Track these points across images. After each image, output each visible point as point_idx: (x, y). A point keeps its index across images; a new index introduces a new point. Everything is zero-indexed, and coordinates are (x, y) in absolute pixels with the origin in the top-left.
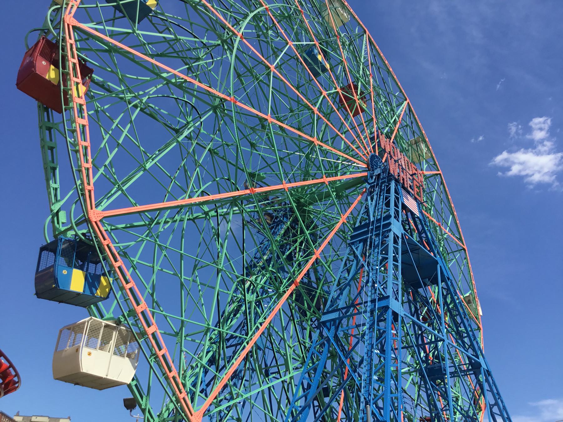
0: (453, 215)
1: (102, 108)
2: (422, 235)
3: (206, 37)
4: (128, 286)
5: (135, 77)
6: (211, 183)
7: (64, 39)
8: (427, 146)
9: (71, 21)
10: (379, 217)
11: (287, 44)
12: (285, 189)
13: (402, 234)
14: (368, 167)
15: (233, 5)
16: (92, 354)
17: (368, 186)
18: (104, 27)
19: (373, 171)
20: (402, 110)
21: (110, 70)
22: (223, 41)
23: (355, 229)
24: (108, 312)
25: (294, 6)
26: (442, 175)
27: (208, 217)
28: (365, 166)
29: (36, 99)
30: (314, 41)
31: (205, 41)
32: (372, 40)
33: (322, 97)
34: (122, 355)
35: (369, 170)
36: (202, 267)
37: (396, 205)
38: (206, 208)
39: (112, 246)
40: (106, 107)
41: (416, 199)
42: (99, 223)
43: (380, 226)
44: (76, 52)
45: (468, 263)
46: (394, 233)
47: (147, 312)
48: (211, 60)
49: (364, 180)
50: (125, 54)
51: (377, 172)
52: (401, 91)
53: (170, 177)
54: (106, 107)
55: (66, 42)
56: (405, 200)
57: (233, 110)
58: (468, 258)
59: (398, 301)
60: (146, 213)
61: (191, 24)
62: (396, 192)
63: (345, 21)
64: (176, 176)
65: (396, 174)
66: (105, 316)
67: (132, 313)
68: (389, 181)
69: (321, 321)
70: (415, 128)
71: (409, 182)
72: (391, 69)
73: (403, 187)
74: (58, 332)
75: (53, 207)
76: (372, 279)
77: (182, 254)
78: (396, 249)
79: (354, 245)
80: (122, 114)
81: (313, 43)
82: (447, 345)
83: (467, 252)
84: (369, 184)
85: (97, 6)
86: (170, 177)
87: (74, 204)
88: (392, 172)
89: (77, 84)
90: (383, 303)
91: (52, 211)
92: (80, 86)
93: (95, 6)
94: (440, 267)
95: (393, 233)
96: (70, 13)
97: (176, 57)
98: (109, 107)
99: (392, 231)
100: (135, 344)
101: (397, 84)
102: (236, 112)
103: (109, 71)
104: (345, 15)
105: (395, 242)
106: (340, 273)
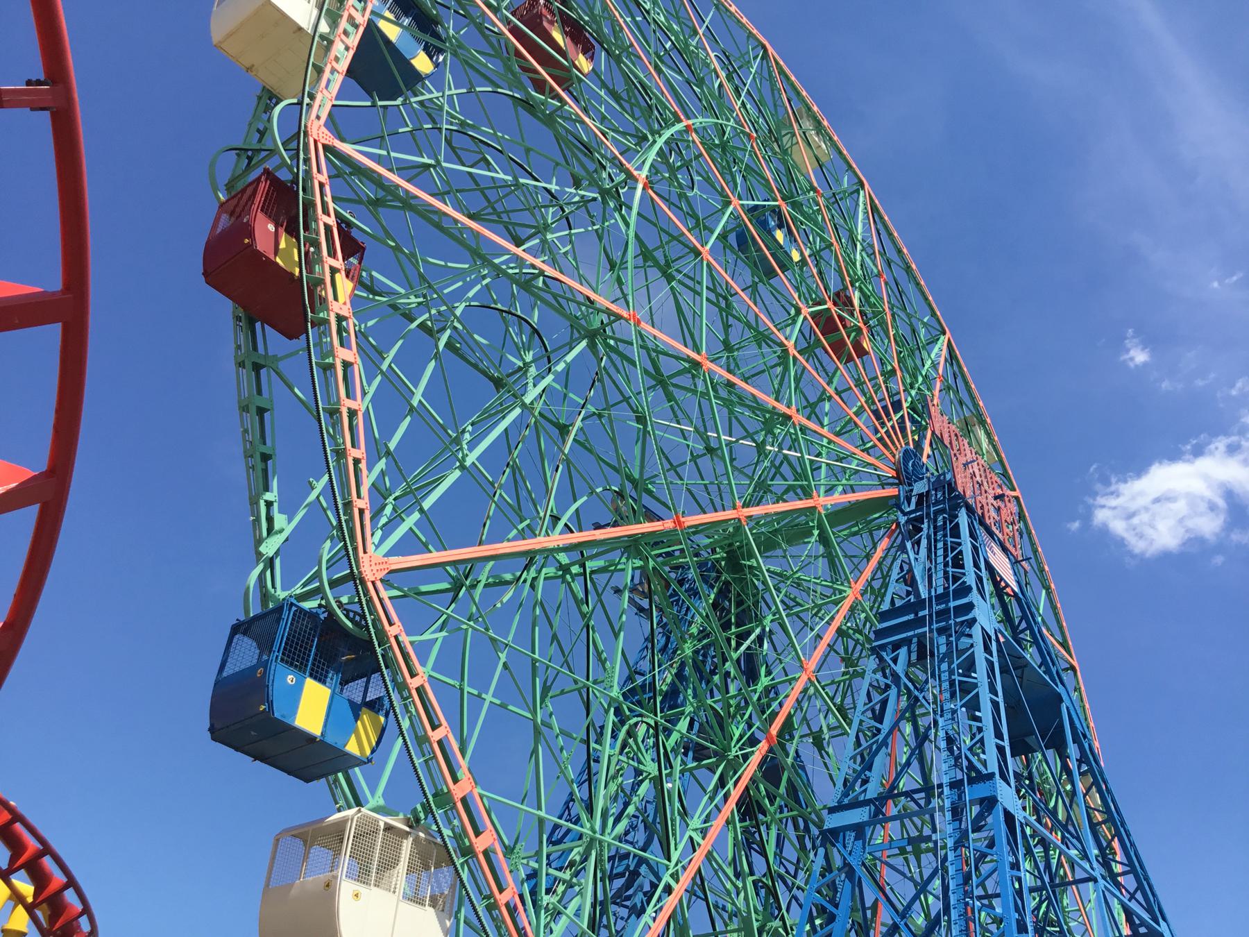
0: (1048, 589)
1: (363, 326)
2: (1021, 636)
3: (554, 180)
4: (435, 736)
5: (443, 263)
6: (585, 498)
7: (308, 173)
8: (988, 435)
9: (321, 135)
10: (940, 591)
11: (730, 203)
12: (739, 520)
13: (995, 630)
14: (898, 477)
15: (606, 118)
16: (362, 898)
17: (903, 520)
18: (388, 153)
19: (910, 485)
20: (939, 350)
21: (393, 244)
22: (604, 193)
23: (883, 616)
24: (373, 793)
25: (732, 123)
26: (1021, 500)
27: (568, 577)
28: (891, 473)
29: (64, 284)
30: (777, 200)
31: (553, 187)
32: (877, 202)
33: (801, 318)
34: (421, 902)
35: (900, 483)
36: (562, 692)
37: (976, 565)
38: (563, 558)
39: (406, 640)
40: (370, 323)
41: (1005, 550)
42: (379, 584)
43: (947, 611)
44: (331, 205)
45: (1082, 701)
46: (982, 628)
47: (473, 798)
48: (567, 232)
49: (893, 504)
50: (428, 214)
51: (920, 487)
52: (933, 314)
53: (492, 484)
54: (370, 323)
55: (312, 179)
56: (990, 554)
57: (634, 341)
58: (1083, 688)
59: (1011, 787)
60: (448, 568)
61: (528, 151)
62: (973, 535)
63: (823, 159)
64: (503, 482)
65: (969, 493)
66: (367, 802)
67: (443, 798)
68: (956, 507)
69: (825, 827)
70: (964, 395)
71: (993, 514)
72: (914, 266)
73: (982, 523)
74: (272, 841)
75: (262, 549)
76: (947, 733)
77: (537, 661)
78: (995, 705)
79: (886, 651)
80: (400, 342)
81: (777, 203)
82: (1103, 892)
83: (1079, 674)
84: (905, 514)
85: (374, 106)
86: (492, 484)
87: (329, 541)
88: (960, 489)
89: (334, 271)
90: (982, 790)
91: (260, 554)
92: (340, 278)
93: (369, 104)
94: (1067, 708)
95: (980, 627)
96: (318, 117)
97: (493, 221)
98: (376, 323)
99: (977, 623)
100: (447, 871)
101: (926, 299)
102: (642, 347)
103: (391, 247)
104: (824, 146)
105: (987, 649)
106: (859, 714)
